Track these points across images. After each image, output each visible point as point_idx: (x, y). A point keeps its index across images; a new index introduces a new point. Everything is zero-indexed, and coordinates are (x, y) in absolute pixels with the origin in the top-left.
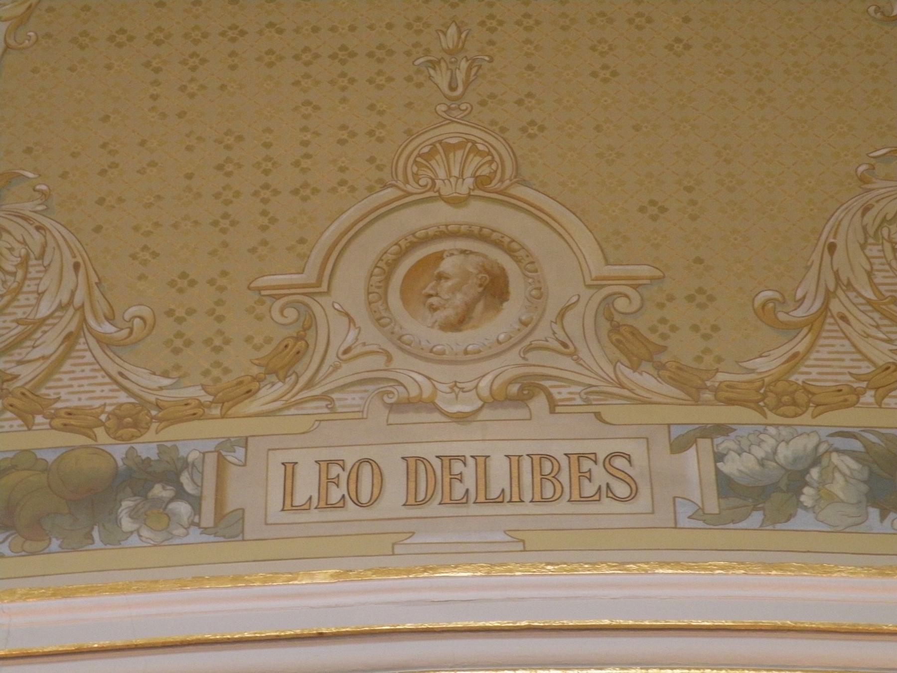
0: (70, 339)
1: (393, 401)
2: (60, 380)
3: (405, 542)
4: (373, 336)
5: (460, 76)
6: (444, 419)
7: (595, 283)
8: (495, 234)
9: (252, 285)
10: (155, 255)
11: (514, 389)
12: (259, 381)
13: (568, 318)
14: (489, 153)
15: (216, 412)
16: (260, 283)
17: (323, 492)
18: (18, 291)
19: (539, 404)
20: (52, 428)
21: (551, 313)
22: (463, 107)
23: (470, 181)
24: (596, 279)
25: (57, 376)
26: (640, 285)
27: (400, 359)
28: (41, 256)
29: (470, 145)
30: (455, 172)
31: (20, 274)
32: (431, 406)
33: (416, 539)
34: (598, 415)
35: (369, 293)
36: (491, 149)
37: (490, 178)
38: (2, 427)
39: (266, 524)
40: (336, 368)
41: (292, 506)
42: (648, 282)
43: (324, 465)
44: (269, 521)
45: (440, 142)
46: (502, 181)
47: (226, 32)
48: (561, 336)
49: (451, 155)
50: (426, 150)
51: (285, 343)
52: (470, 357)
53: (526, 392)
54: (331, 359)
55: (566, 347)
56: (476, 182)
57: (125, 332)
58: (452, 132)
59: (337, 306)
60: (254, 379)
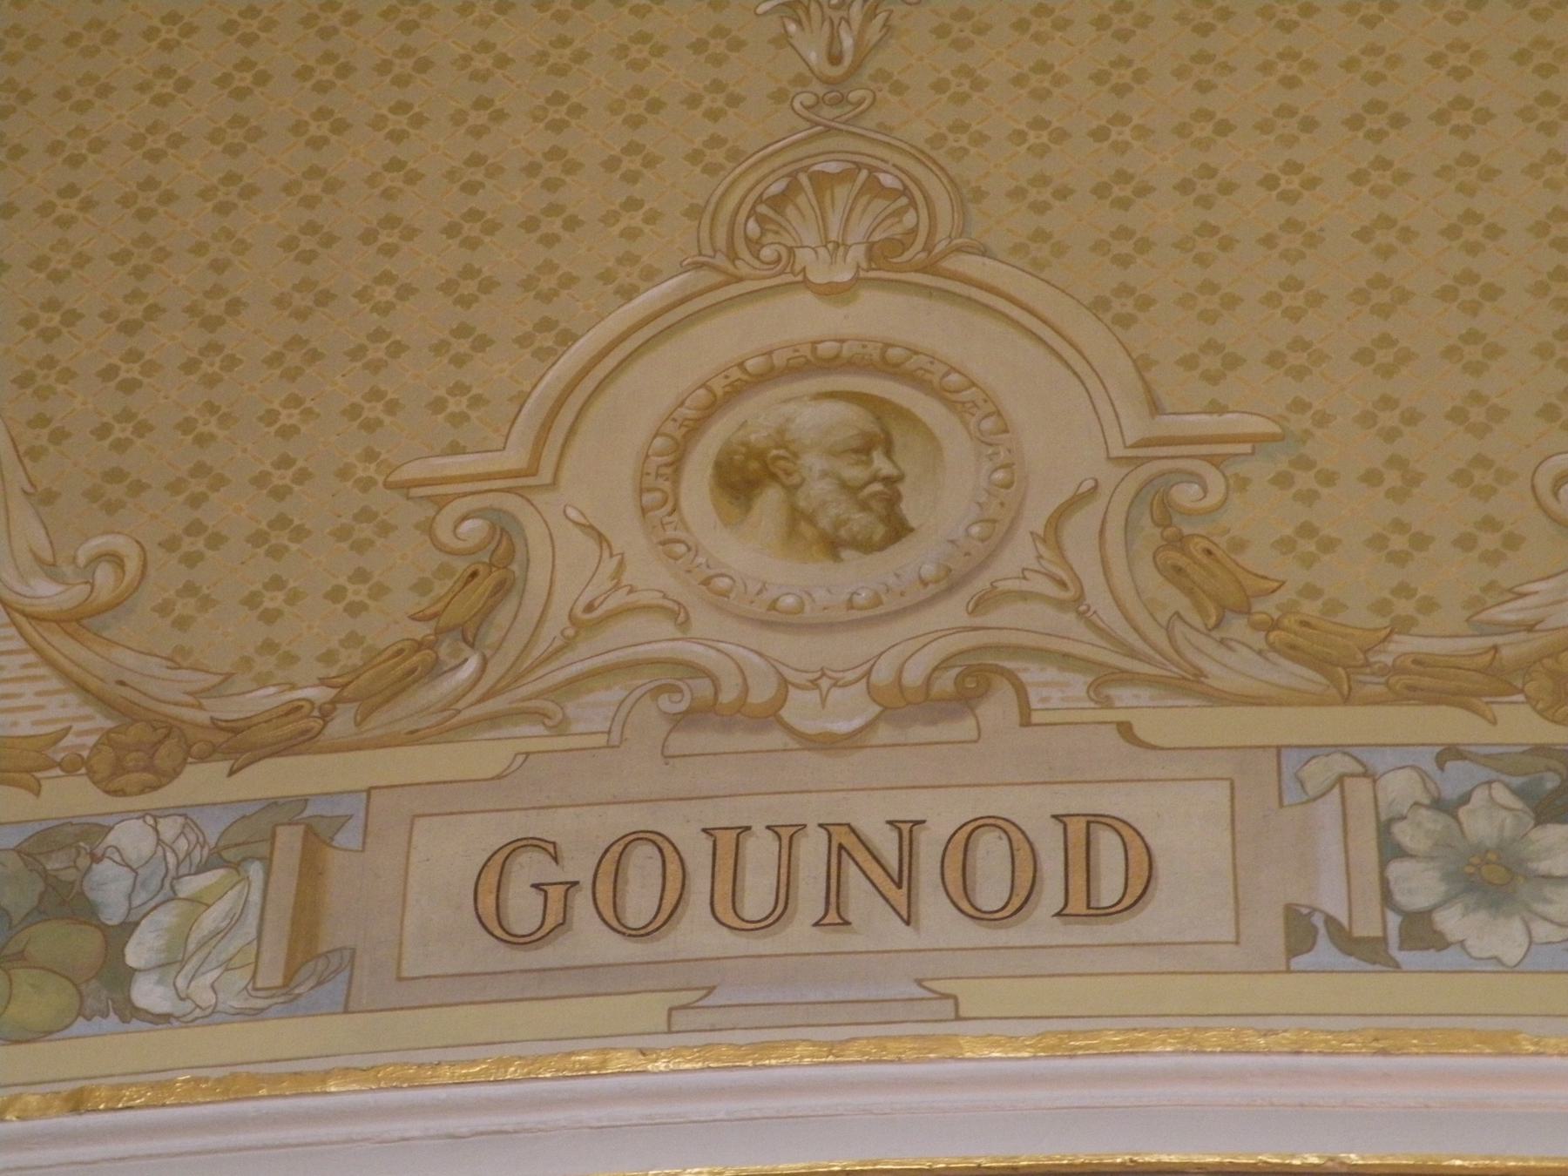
3: (700, 1004)
4: (651, 576)
9: (391, 479)
10: (392, 407)
11: (946, 683)
14: (905, 191)
19: (997, 709)
21: (1036, 517)
22: (854, 96)
23: (857, 253)
27: (704, 621)
29: (864, 174)
32: (769, 717)
34: (1125, 730)
39: (400, 979)
40: (568, 644)
41: (1089, 907)
44: (405, 974)
46: (928, 248)
51: (1200, 556)
56: (870, 255)
59: (572, 513)
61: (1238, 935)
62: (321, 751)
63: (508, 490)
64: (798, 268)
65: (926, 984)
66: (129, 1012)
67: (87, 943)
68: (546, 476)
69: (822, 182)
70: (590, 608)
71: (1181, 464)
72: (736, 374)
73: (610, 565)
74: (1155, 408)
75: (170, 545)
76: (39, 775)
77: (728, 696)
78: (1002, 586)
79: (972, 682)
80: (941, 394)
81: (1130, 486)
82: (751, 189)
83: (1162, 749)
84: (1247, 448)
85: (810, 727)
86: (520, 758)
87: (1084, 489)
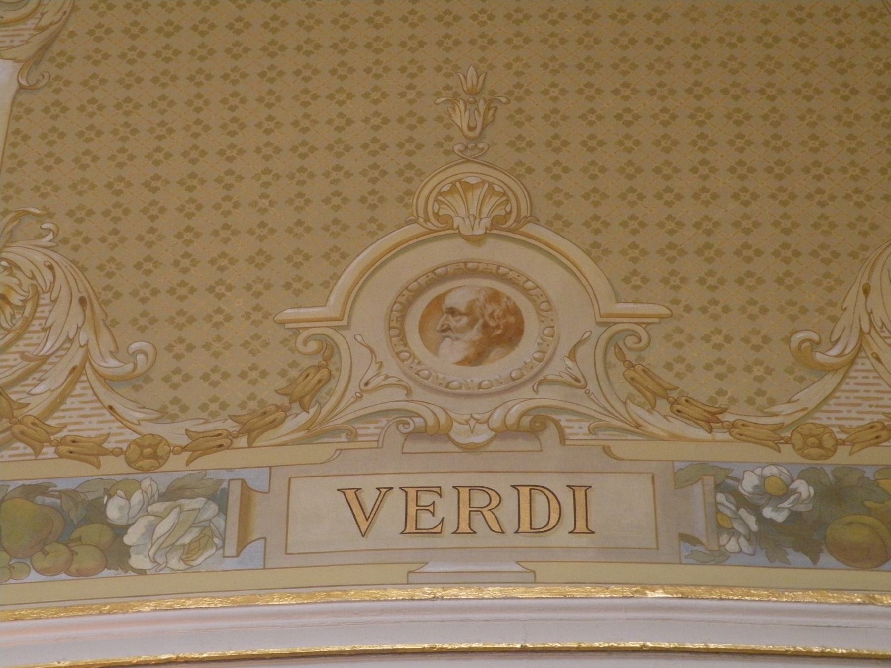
0: (76, 372)
4: (393, 368)
6: (457, 450)
7: (606, 320)
8: (511, 273)
11: (526, 420)
12: (285, 412)
13: (581, 352)
14: (504, 194)
15: (243, 441)
18: (27, 323)
19: (550, 435)
20: (61, 456)
21: (564, 349)
22: (481, 146)
27: (419, 393)
28: (51, 290)
30: (473, 211)
33: (427, 568)
34: (607, 451)
35: (390, 328)
36: (508, 191)
38: (2, 457)
40: (359, 398)
42: (657, 320)
43: (412, 493)
45: (460, 181)
47: (370, 94)
50: (445, 189)
52: (479, 392)
53: (538, 424)
54: (353, 389)
55: (578, 383)
57: (130, 367)
58: (471, 173)
59: (359, 338)
60: (278, 408)
61: (657, 544)
64: (455, 226)
66: (126, 567)
67: (107, 536)
70: (367, 384)
72: (522, 279)
75: (170, 348)
78: (550, 377)
79: (535, 425)
81: (606, 336)
83: (623, 460)
84: (657, 320)
86: (338, 452)
87: (585, 336)
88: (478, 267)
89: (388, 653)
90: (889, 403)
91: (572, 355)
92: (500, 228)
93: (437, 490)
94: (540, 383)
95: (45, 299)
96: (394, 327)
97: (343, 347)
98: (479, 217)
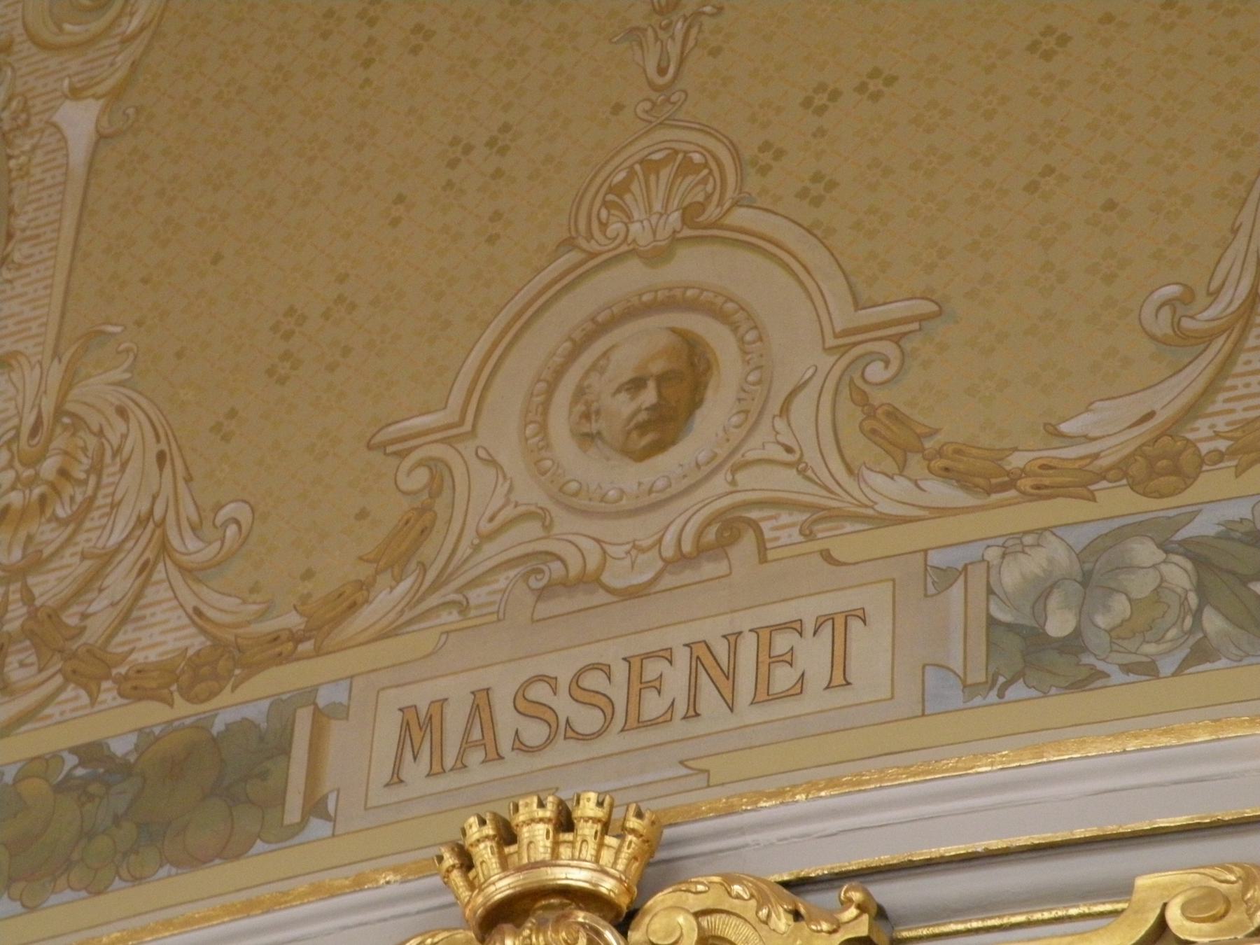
0: (146, 568)
1: (541, 584)
2: (1234, 388)
5: (674, 50)
11: (711, 535)
16: (379, 438)
17: (634, 699)
24: (846, 333)
25: (1229, 383)
26: (905, 334)
27: (565, 523)
29: (680, 156)
30: (657, 207)
31: (92, 480)
34: (827, 556)
37: (702, 206)
39: (892, 698)
40: (476, 548)
43: (765, 635)
48: (786, 439)
49: (653, 178)
53: (726, 535)
59: (482, 453)
62: (298, 659)
63: (881, 339)
65: (690, 763)
68: (467, 427)
69: (651, 167)
71: (869, 347)
73: (502, 489)
74: (858, 306)
76: (1092, 488)
77: (575, 569)
80: (721, 316)
82: (605, 181)
84: (915, 326)
85: (618, 584)
86: (444, 637)
87: (807, 376)
88: (656, 298)
89: (1022, 852)
90: (1255, 389)
91: (785, 410)
92: (697, 225)
93: (667, 654)
94: (735, 470)
95: (111, 468)
96: (531, 422)
97: (459, 471)
98: (665, 213)
